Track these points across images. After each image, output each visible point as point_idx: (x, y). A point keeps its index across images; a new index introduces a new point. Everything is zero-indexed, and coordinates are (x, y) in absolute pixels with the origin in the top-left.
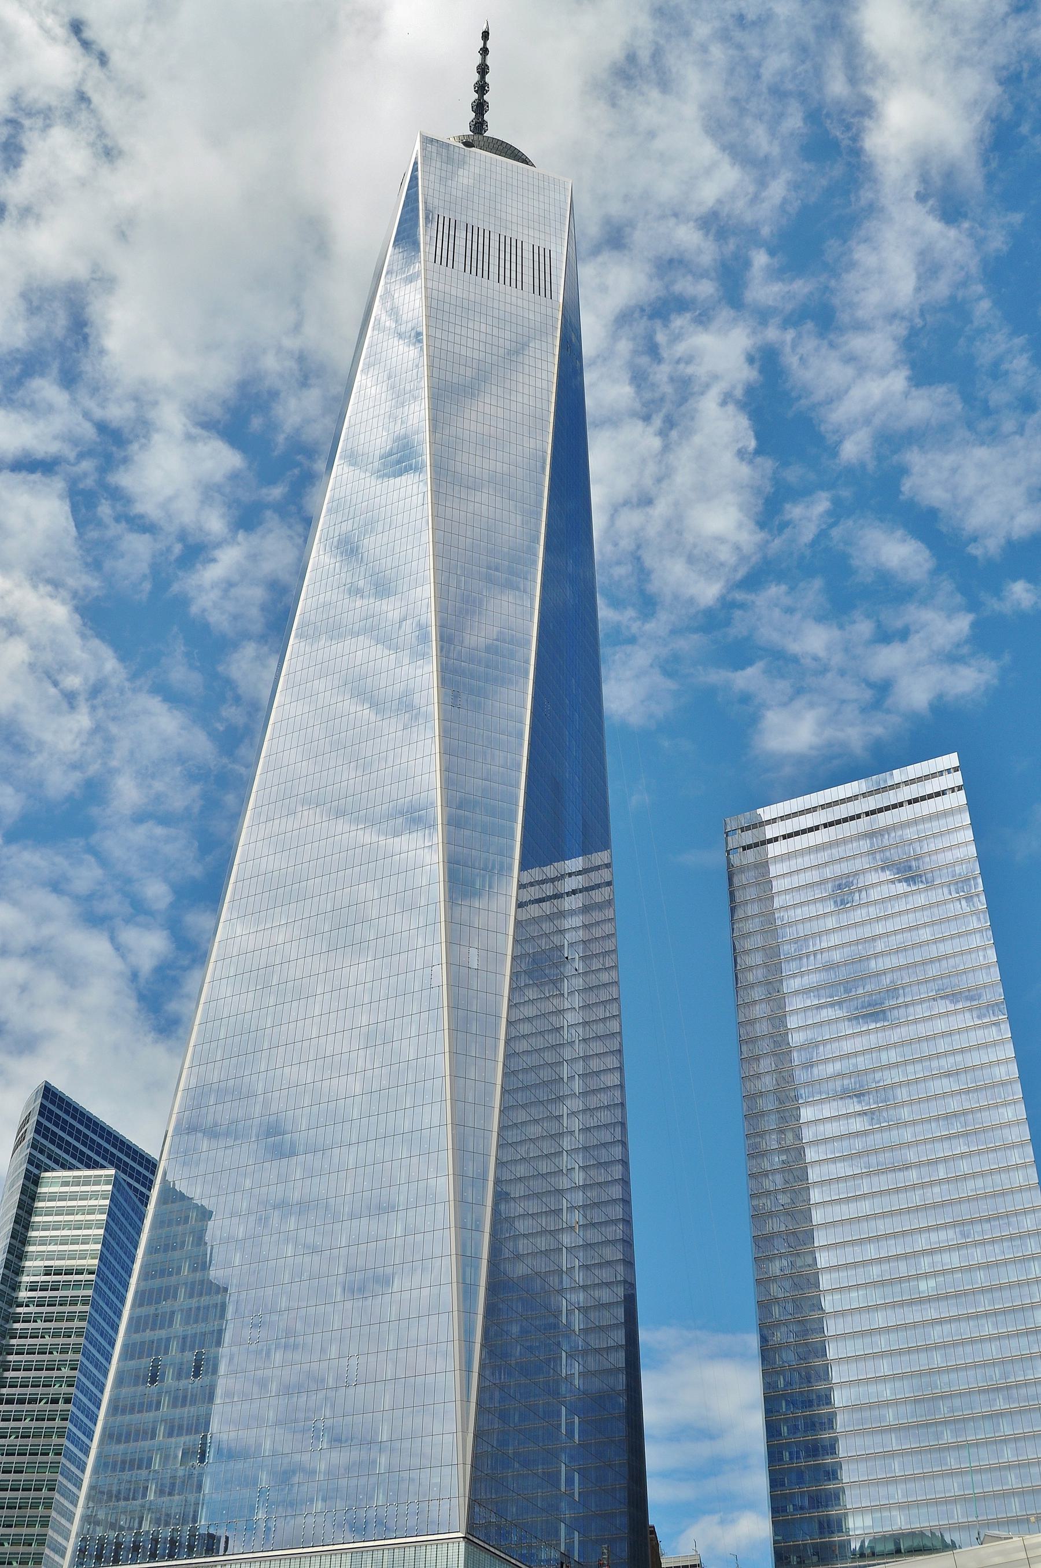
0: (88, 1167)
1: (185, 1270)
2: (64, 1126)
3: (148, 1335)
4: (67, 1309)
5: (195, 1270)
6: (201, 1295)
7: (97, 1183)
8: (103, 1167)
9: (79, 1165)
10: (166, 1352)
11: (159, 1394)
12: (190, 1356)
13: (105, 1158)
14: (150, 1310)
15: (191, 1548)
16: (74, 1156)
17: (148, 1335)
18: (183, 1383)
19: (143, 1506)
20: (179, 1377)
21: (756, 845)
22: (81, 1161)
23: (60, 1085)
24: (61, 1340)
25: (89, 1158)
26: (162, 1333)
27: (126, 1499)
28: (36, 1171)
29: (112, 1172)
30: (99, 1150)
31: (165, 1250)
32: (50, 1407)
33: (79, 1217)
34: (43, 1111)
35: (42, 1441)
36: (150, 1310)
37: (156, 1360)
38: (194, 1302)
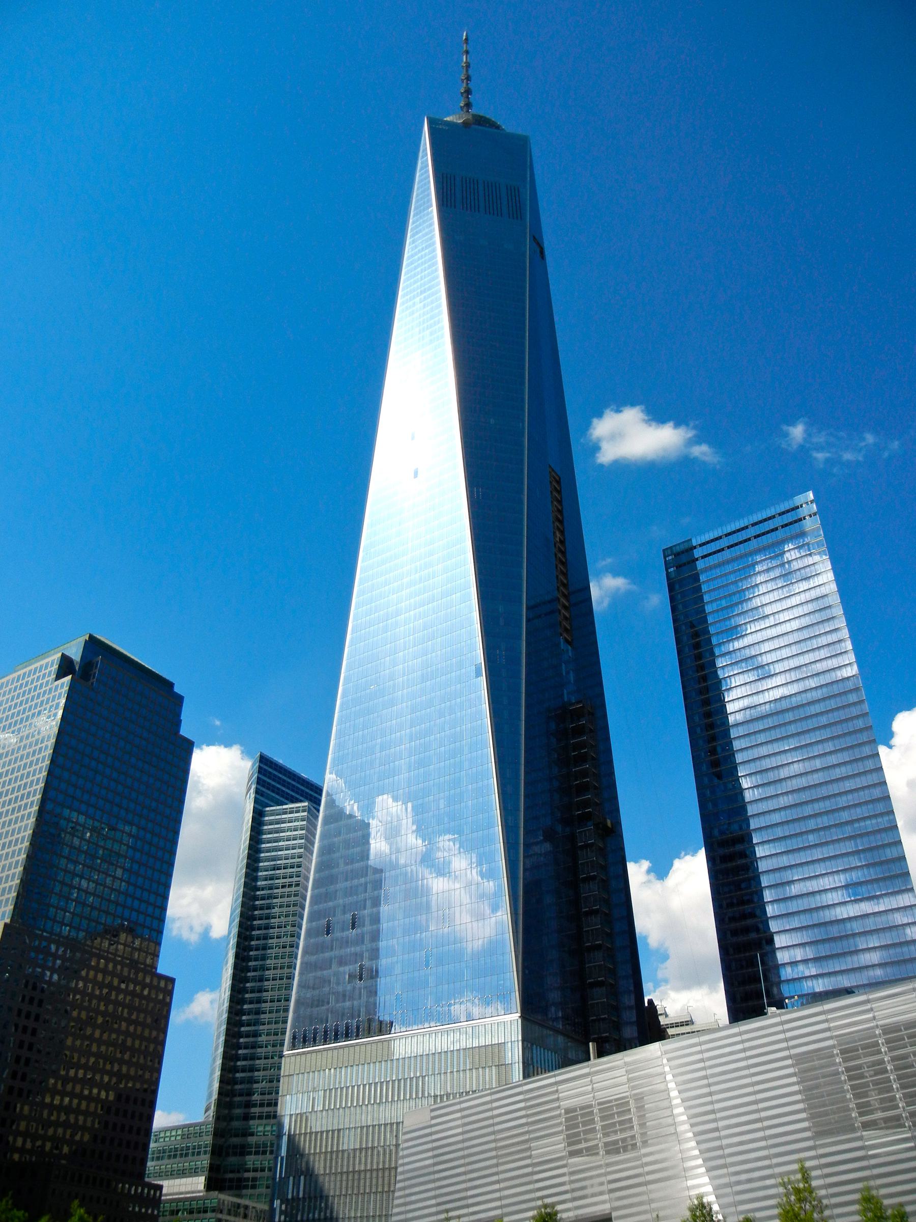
0: (293, 802)
1: (342, 865)
2: (274, 778)
3: (322, 906)
4: (287, 890)
5: (347, 864)
6: (352, 879)
7: (297, 812)
8: (301, 801)
9: (301, 798)
10: (334, 916)
11: (332, 941)
12: (349, 916)
13: (302, 795)
14: (323, 890)
15: (336, 1035)
16: (283, 796)
17: (322, 906)
18: (345, 934)
19: (328, 1010)
20: (343, 930)
21: (796, 522)
22: (287, 799)
23: (269, 754)
24: (285, 909)
25: (292, 796)
26: (362, 897)
27: (317, 1006)
28: (260, 808)
29: (306, 804)
30: (297, 791)
31: (329, 854)
32: (282, 950)
33: (289, 833)
34: (260, 770)
35: (279, 971)
36: (323, 890)
37: (354, 915)
38: (348, 884)
